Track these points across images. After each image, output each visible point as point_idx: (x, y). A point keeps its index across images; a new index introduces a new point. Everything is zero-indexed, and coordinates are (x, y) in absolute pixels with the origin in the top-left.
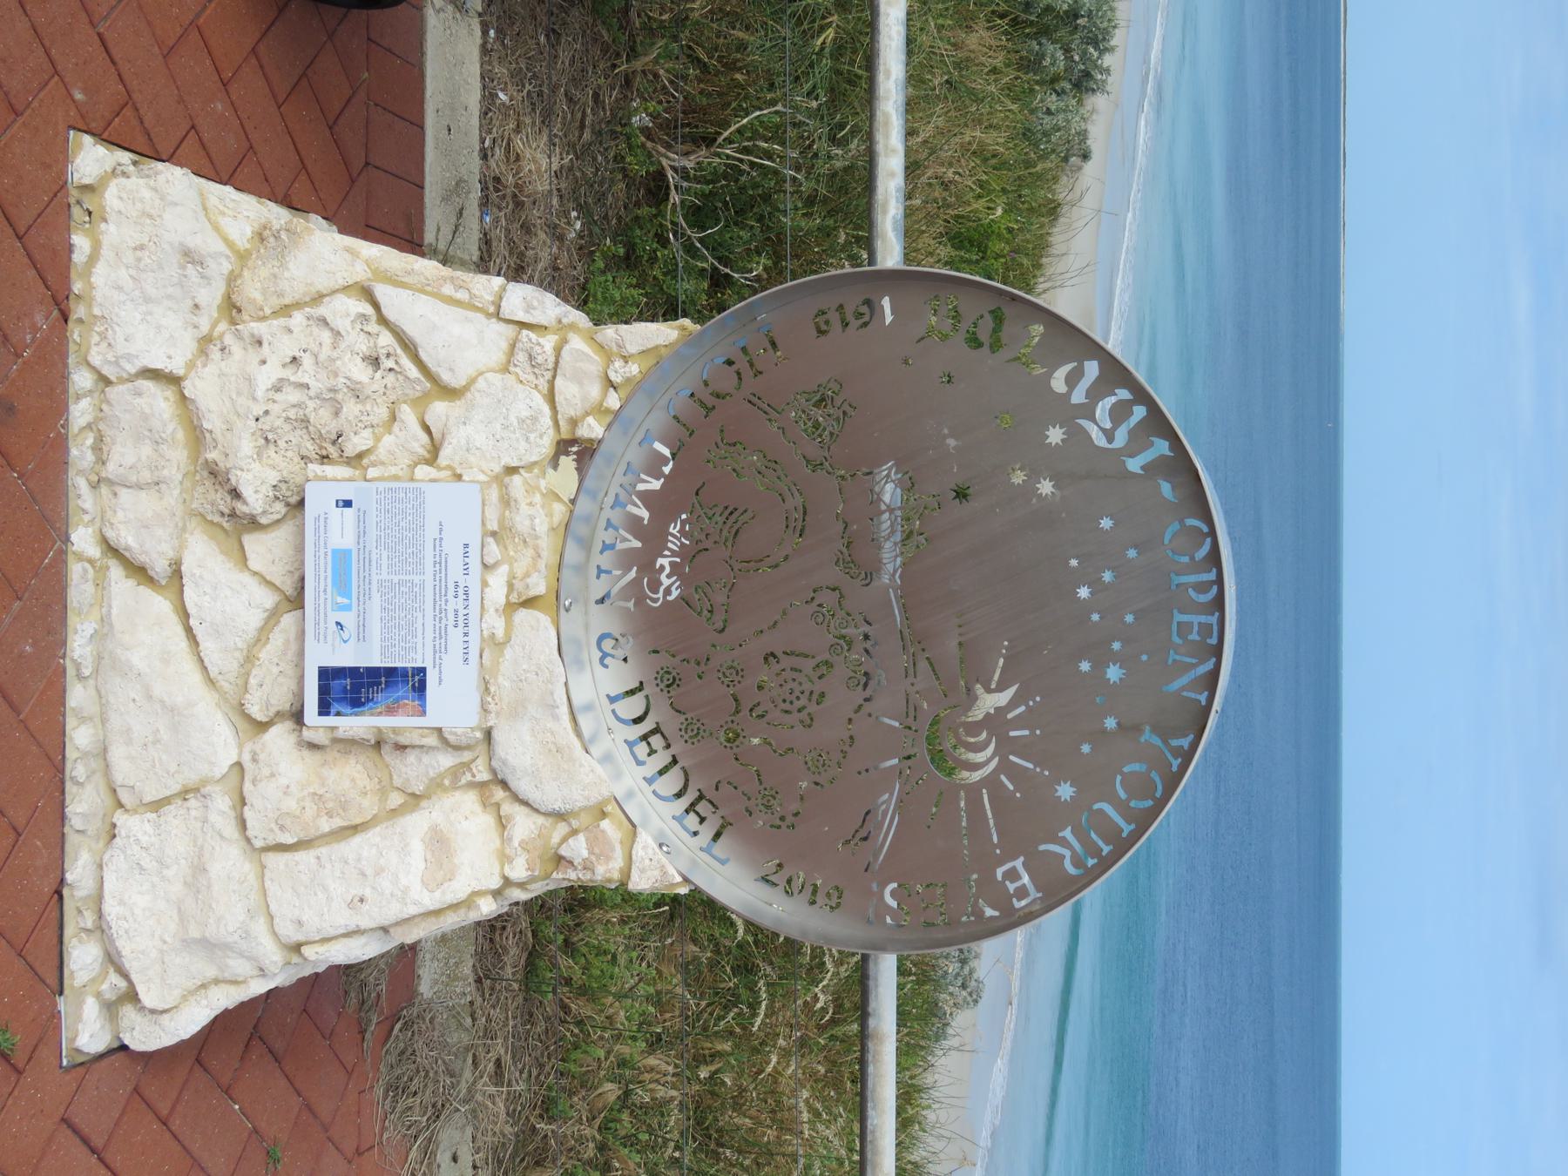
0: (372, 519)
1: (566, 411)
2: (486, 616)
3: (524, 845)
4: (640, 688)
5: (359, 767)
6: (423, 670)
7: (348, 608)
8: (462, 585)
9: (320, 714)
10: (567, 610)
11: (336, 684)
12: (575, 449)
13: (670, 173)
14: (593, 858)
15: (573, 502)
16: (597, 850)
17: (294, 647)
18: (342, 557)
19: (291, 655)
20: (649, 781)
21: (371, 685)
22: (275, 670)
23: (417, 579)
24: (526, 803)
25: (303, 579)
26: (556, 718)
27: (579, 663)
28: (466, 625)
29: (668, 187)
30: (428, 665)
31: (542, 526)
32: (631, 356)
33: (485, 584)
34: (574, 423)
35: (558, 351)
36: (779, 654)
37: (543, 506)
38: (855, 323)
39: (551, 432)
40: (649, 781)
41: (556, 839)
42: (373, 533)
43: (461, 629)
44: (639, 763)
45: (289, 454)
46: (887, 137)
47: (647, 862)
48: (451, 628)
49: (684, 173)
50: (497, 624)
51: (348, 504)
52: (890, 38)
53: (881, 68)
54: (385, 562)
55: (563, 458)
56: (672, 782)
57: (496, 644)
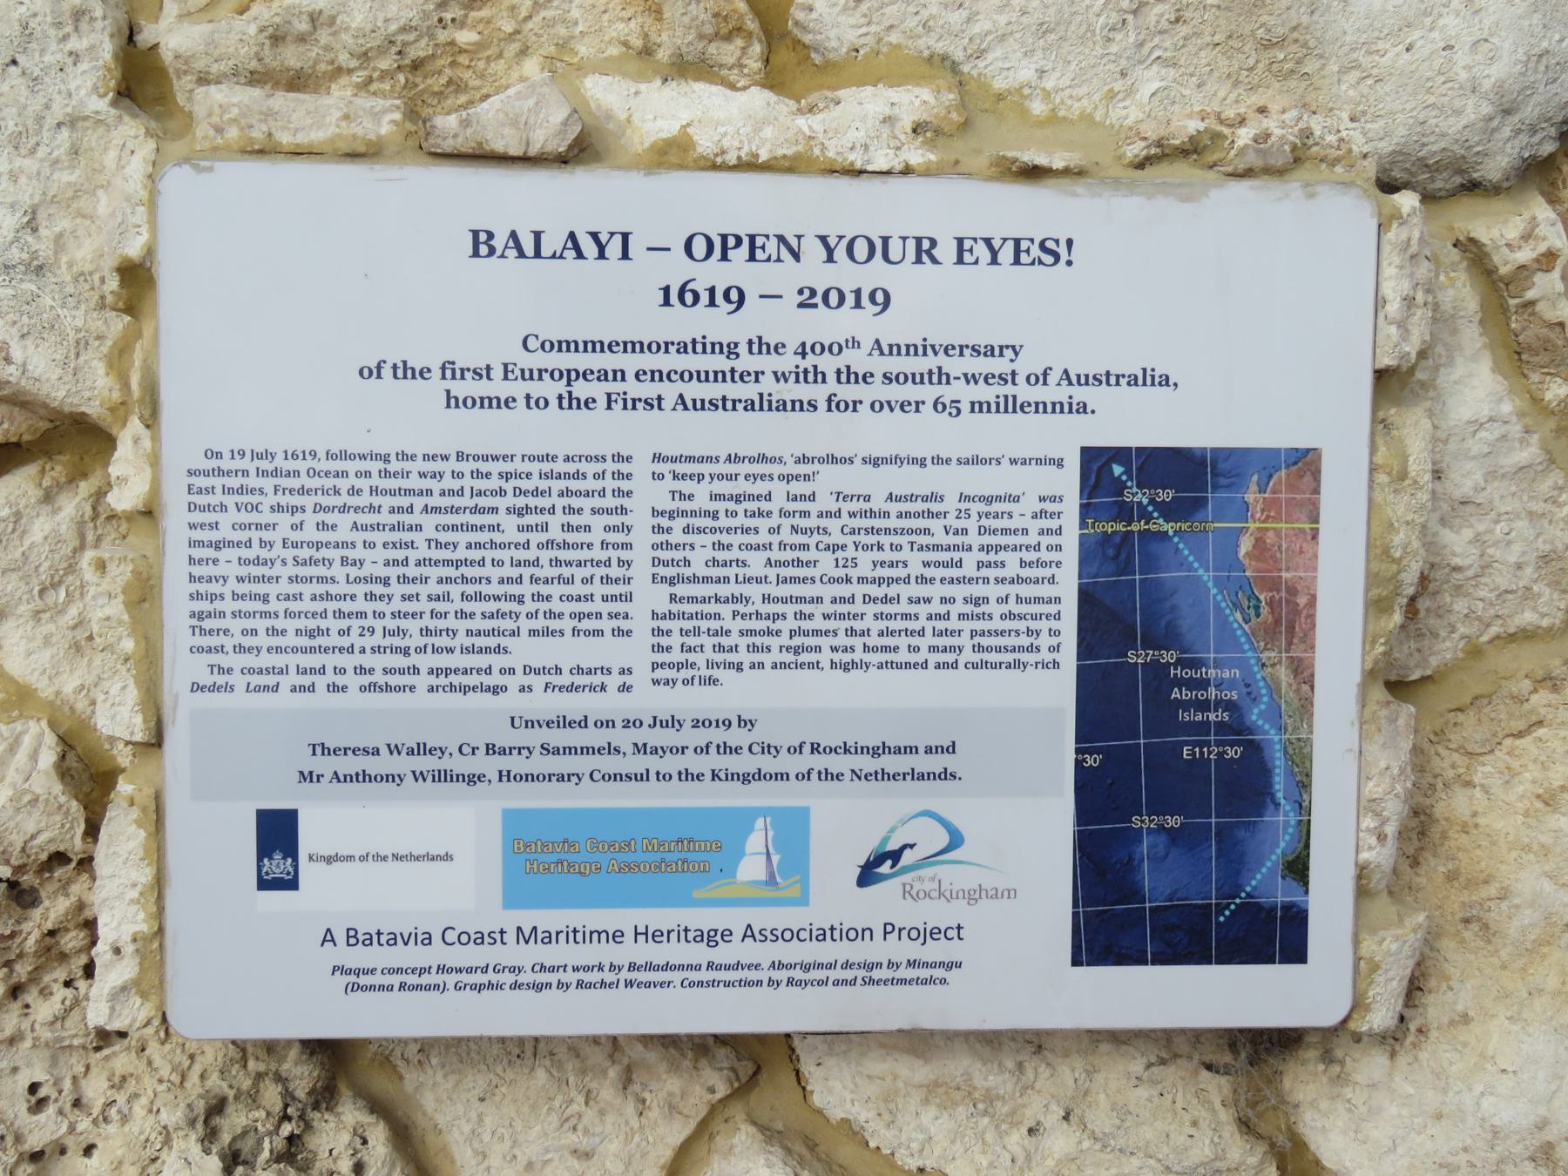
0: (360, 714)
2: (834, 150)
5: (1484, 772)
6: (1096, 462)
7: (792, 832)
8: (677, 270)
9: (1296, 952)
11: (1158, 880)
17: (959, 1066)
18: (544, 859)
19: (990, 1077)
21: (1164, 714)
22: (1060, 1141)
23: (649, 495)
25: (669, 1042)
28: (880, 249)
30: (1068, 438)
33: (674, 154)
42: (423, 712)
43: (902, 279)
45: (96, 1090)
48: (892, 328)
50: (858, 118)
51: (277, 832)
54: (567, 651)
57: (971, 128)
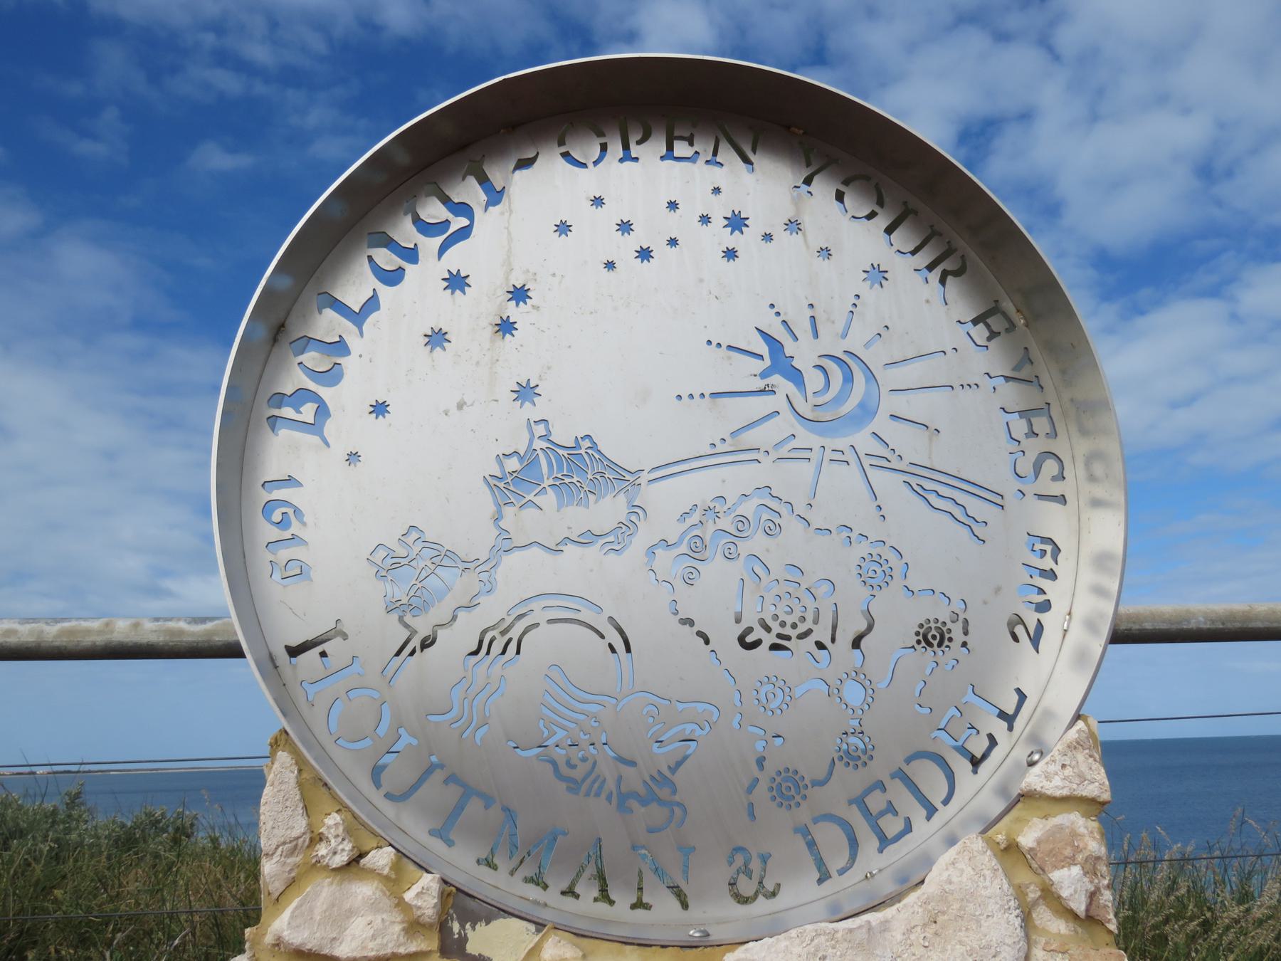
4: (804, 831)
12: (456, 927)
14: (1080, 857)
15: (540, 926)
16: (1068, 852)
20: (931, 811)
26: (885, 926)
32: (310, 827)
34: (414, 926)
36: (739, 630)
38: (295, 528)
40: (931, 811)
41: (1059, 926)
44: (908, 828)
47: (1068, 771)
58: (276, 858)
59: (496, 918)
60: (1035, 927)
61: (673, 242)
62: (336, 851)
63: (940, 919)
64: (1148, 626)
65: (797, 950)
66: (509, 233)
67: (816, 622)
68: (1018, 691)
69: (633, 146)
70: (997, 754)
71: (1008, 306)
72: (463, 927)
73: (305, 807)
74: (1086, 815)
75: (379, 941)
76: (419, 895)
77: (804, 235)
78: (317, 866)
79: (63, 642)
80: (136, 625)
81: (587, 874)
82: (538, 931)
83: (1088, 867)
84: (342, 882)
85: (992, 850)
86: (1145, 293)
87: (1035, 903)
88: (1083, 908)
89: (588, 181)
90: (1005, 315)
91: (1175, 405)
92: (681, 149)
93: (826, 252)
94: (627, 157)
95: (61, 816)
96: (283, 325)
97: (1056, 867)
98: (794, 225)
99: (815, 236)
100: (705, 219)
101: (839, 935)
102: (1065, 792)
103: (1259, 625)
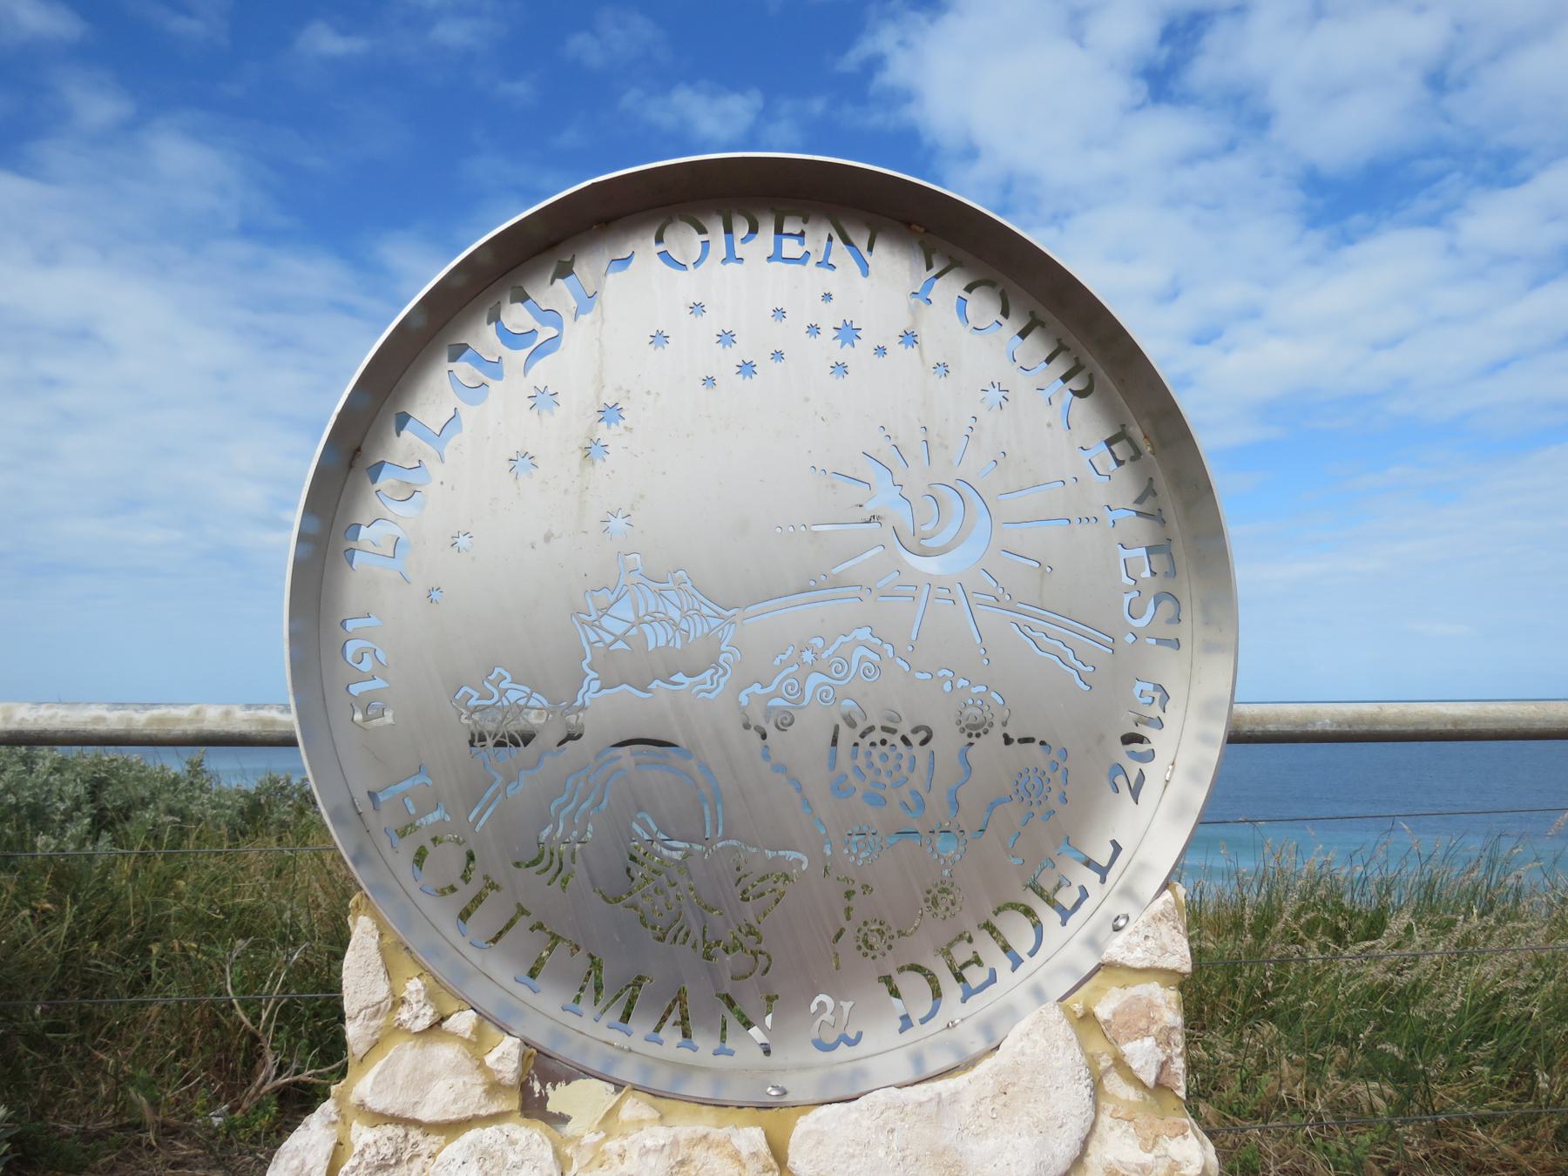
1: (474, 1100)
3: (1150, 1143)
4: (887, 980)
10: (785, 1093)
12: (537, 1087)
13: (281, 1081)
14: (1154, 1029)
15: (619, 1086)
16: (1143, 1024)
20: (1017, 962)
24: (1085, 1144)
26: (955, 1097)
27: (859, 1074)
29: (296, 1084)
31: (658, 1136)
32: (392, 991)
34: (495, 1088)
35: (380, 1118)
37: (625, 1136)
39: (507, 1127)
40: (1017, 962)
41: (1129, 1093)
44: (993, 978)
46: (178, 720)
47: (1150, 943)
49: (281, 1069)
52: (51, 718)
53: (90, 727)
55: (552, 1107)
56: (1019, 932)
58: (359, 1021)
59: (576, 1077)
60: (1105, 1093)
61: (778, 355)
62: (417, 1015)
63: (1010, 1090)
64: (1272, 728)
65: (865, 1123)
66: (601, 345)
67: (912, 769)
68: (1114, 843)
69: (737, 245)
70: (1086, 907)
71: (1136, 431)
72: (543, 1086)
73: (387, 972)
74: (1165, 985)
75: (460, 1104)
76: (499, 1059)
77: (921, 349)
78: (399, 1029)
79: (152, 730)
80: (227, 714)
81: (671, 1019)
82: (617, 1091)
83: (1162, 1037)
84: (424, 1043)
85: (1068, 1018)
86: (1358, 220)
87: (1107, 1071)
88: (1153, 1078)
89: (686, 285)
90: (1131, 442)
91: (1377, 346)
92: (791, 247)
93: (943, 368)
94: (731, 257)
95: (182, 785)
96: (359, 449)
97: (1129, 1039)
98: (909, 338)
99: (932, 349)
100: (814, 330)
101: (908, 1108)
102: (1146, 964)
103: (1387, 728)
